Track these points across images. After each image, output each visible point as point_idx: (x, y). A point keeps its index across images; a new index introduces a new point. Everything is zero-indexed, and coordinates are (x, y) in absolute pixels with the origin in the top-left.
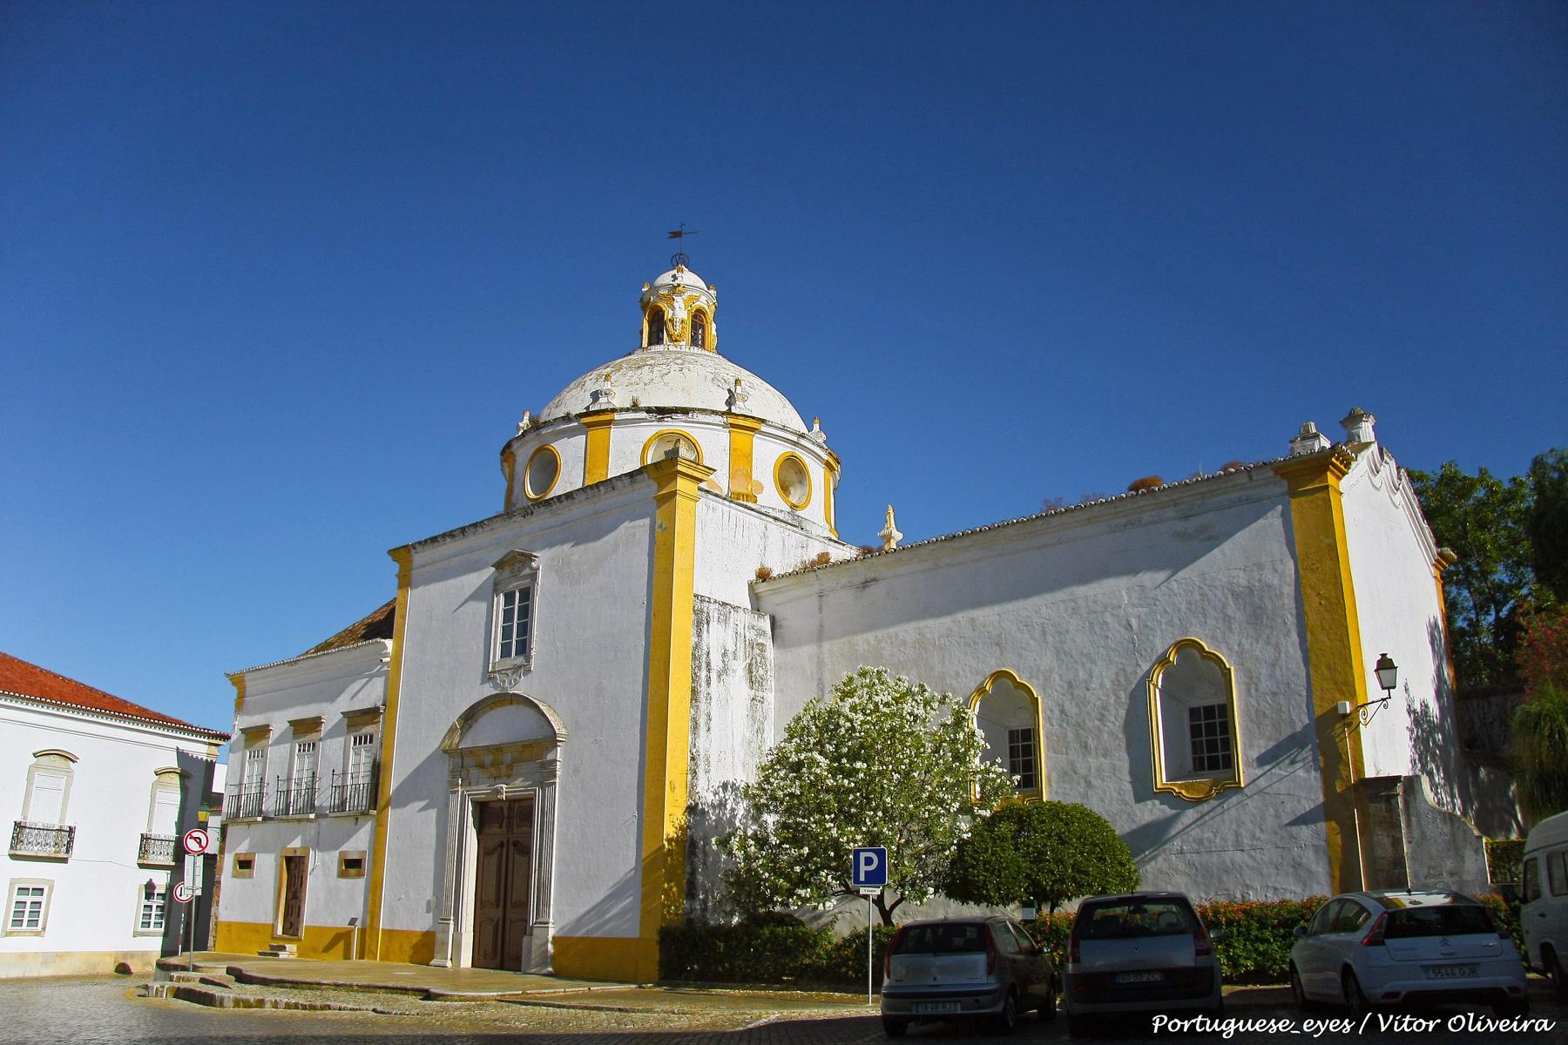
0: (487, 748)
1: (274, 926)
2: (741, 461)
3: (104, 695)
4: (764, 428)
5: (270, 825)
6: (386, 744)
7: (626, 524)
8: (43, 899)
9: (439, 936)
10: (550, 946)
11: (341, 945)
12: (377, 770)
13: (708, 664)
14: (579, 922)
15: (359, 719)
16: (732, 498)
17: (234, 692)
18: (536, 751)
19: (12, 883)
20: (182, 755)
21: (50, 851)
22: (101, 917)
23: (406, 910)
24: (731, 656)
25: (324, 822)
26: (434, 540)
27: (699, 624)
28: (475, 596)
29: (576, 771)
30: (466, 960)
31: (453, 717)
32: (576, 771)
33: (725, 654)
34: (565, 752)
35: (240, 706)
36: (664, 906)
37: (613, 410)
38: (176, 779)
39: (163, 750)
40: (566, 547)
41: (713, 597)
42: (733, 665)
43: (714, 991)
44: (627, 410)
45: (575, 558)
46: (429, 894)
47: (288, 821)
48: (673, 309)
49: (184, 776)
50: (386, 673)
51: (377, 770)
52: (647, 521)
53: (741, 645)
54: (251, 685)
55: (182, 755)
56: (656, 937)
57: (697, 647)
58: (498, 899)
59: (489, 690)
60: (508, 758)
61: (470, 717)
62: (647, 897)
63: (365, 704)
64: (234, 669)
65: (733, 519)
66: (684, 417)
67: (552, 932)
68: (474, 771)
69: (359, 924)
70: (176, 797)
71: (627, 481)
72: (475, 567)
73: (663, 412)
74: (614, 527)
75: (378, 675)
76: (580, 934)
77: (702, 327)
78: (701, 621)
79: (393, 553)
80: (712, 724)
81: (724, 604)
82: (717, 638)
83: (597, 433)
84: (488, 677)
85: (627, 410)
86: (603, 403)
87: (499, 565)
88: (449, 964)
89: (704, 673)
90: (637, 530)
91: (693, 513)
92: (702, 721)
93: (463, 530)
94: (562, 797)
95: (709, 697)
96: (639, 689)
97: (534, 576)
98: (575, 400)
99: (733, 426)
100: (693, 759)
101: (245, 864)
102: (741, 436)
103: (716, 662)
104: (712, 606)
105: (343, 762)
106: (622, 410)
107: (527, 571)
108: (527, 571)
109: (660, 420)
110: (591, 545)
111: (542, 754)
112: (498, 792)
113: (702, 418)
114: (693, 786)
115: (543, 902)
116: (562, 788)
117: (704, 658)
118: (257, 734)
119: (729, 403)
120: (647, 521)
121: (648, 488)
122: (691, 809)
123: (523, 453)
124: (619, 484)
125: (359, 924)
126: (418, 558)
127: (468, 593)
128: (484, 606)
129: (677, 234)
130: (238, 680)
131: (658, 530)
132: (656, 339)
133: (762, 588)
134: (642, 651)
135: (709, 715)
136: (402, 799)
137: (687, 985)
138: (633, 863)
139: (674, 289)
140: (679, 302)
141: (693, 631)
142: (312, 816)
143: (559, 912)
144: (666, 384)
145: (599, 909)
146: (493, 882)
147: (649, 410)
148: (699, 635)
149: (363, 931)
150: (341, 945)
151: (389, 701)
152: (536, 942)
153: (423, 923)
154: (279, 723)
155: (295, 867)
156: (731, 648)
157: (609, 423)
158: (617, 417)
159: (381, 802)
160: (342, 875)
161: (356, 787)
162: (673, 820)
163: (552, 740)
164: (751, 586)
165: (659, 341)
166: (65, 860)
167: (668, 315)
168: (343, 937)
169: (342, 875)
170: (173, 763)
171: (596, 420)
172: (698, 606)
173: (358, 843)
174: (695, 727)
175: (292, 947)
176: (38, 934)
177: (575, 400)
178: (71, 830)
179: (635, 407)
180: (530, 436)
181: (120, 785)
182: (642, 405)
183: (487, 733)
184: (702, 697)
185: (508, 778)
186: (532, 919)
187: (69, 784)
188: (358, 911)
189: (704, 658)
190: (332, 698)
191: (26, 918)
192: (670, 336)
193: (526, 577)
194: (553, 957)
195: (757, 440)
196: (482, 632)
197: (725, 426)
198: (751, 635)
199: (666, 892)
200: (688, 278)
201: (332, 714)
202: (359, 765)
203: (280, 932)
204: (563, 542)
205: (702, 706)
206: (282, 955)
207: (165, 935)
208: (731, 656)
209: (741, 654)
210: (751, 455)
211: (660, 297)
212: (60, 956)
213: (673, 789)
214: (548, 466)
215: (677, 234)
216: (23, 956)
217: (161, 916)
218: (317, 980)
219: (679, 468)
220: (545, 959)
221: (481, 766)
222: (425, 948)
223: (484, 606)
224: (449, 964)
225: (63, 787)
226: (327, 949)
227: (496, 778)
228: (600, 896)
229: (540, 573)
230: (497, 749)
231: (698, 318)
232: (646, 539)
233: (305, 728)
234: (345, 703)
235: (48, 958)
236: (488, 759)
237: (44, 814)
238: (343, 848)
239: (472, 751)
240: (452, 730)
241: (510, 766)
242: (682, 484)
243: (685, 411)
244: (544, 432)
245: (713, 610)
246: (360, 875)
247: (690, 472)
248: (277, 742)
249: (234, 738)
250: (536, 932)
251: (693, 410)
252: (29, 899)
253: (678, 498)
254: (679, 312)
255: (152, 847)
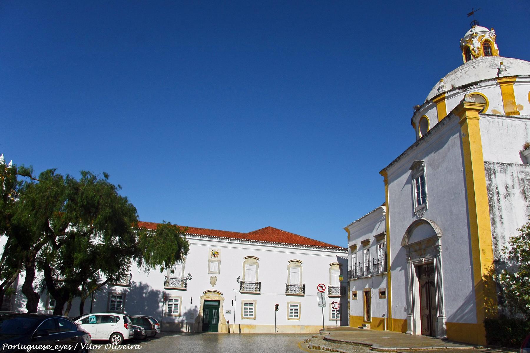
0: (416, 243)
1: (364, 317)
2: (508, 98)
3: (313, 240)
4: (517, 80)
5: (360, 281)
6: (388, 247)
7: (451, 138)
8: (179, 303)
9: (408, 321)
10: (444, 326)
11: (382, 325)
12: (386, 256)
13: (498, 193)
14: (455, 315)
15: (380, 237)
16: (508, 115)
17: (347, 234)
18: (430, 244)
19: (288, 303)
20: (338, 258)
21: (298, 293)
22: (317, 316)
23: (398, 313)
24: (510, 187)
25: (374, 278)
26: (391, 164)
27: (489, 175)
28: (407, 183)
29: (447, 249)
30: (419, 332)
31: (403, 232)
32: (447, 249)
33: (507, 187)
34: (442, 241)
35: (349, 239)
36: (485, 308)
37: (444, 93)
38: (338, 267)
39: (332, 257)
40: (432, 154)
41: (496, 161)
42: (512, 191)
43: (174, 336)
44: (450, 91)
45: (436, 158)
46: (405, 305)
47: (364, 278)
48: (473, 44)
49: (340, 265)
50: (385, 219)
51: (386, 256)
52: (458, 134)
53: (516, 181)
54: (351, 231)
55: (338, 258)
56: (483, 324)
57: (489, 185)
58: (427, 306)
59: (415, 219)
60: (423, 247)
61: (410, 231)
62: (478, 305)
63: (380, 232)
64: (345, 227)
65: (505, 124)
66: (476, 86)
67: (445, 320)
68: (414, 253)
69: (386, 316)
70: (339, 273)
71: (447, 119)
72: (405, 172)
73: (465, 87)
74: (447, 141)
75: (383, 220)
76: (454, 321)
77: (490, 47)
78: (490, 173)
79: (380, 172)
80: (504, 221)
81: (503, 164)
82: (500, 180)
83: (440, 105)
84: (414, 215)
85: (450, 91)
86: (441, 91)
87: (412, 168)
88: (412, 333)
89: (495, 197)
90: (455, 139)
91: (477, 126)
92: (497, 220)
93: (399, 158)
94: (443, 261)
95: (500, 208)
96: (465, 209)
97: (423, 170)
98: (433, 93)
99: (501, 83)
100: (494, 238)
101: (355, 295)
102: (506, 87)
103: (502, 191)
104: (496, 166)
105: (376, 253)
106: (448, 92)
107: (421, 168)
108: (421, 168)
109: (465, 91)
110: (440, 151)
111: (434, 244)
112: (421, 261)
113: (484, 84)
114: (496, 251)
115: (441, 308)
116: (443, 257)
117: (494, 191)
118: (354, 247)
119: (498, 74)
120: (458, 134)
121: (456, 119)
122: (497, 262)
123: (417, 121)
124: (445, 122)
125: (386, 316)
126: (389, 172)
127: (405, 181)
128: (410, 185)
129: (470, 14)
130: (347, 230)
131: (463, 137)
132: (468, 59)
133: (527, 153)
134: (464, 191)
135: (501, 217)
136: (394, 268)
137: (498, 348)
138: (471, 289)
139: (472, 36)
140: (475, 41)
141: (486, 178)
142: (369, 276)
143: (446, 311)
144: (467, 75)
145: (461, 309)
146: (425, 299)
147: (459, 88)
148: (490, 179)
149: (387, 319)
150: (382, 325)
151: (387, 230)
152: (439, 324)
153: (403, 316)
154: (358, 243)
155: (367, 294)
156: (510, 183)
157: (444, 99)
158: (446, 95)
159: (388, 269)
160: (380, 298)
161: (381, 264)
162: (486, 266)
163: (435, 238)
164: (521, 153)
165: (470, 59)
166: (303, 296)
167: (471, 47)
168: (382, 321)
169: (380, 298)
170: (336, 261)
171: (440, 98)
172: (488, 166)
173: (383, 286)
174: (494, 223)
175: (368, 325)
176: (298, 319)
177: (433, 93)
178: (304, 286)
179: (454, 89)
180: (417, 114)
181: (319, 268)
182: (457, 85)
183: (416, 237)
184: (496, 208)
185: (424, 255)
186: (438, 315)
187: (301, 271)
188: (385, 312)
189: (494, 191)
190: (371, 231)
191: (294, 314)
192: (474, 56)
193: (421, 170)
194: (446, 330)
195: (515, 86)
196: (411, 197)
197: (497, 84)
198: (522, 176)
199: (486, 302)
200: (477, 29)
201: (371, 237)
202: (381, 254)
203: (366, 319)
204: (431, 153)
205: (497, 212)
206: (365, 328)
207: (341, 320)
208: (510, 187)
209: (517, 185)
210: (513, 94)
211: (467, 42)
212: (307, 327)
213: (484, 253)
214: (425, 122)
215: (470, 14)
216: (294, 326)
217: (339, 314)
218: (338, 339)
219: (465, 107)
220: (444, 332)
221: (415, 251)
222: (405, 326)
223: (410, 185)
224: (412, 333)
225: (255, 269)
226: (378, 326)
227: (421, 255)
228: (461, 304)
229: (425, 168)
230: (419, 243)
231: (486, 46)
232: (459, 143)
233: (365, 243)
234: (375, 233)
235: (302, 327)
236: (417, 248)
237: (295, 281)
238: (380, 288)
239: (412, 245)
240: (404, 237)
241: (424, 250)
242: (468, 114)
243: (476, 83)
244: (421, 111)
245: (497, 168)
246: (385, 298)
247: (472, 107)
248: (359, 250)
249: (349, 250)
250: (439, 320)
251: (479, 82)
252: (294, 308)
253: (468, 120)
254: (476, 45)
255: (333, 290)
